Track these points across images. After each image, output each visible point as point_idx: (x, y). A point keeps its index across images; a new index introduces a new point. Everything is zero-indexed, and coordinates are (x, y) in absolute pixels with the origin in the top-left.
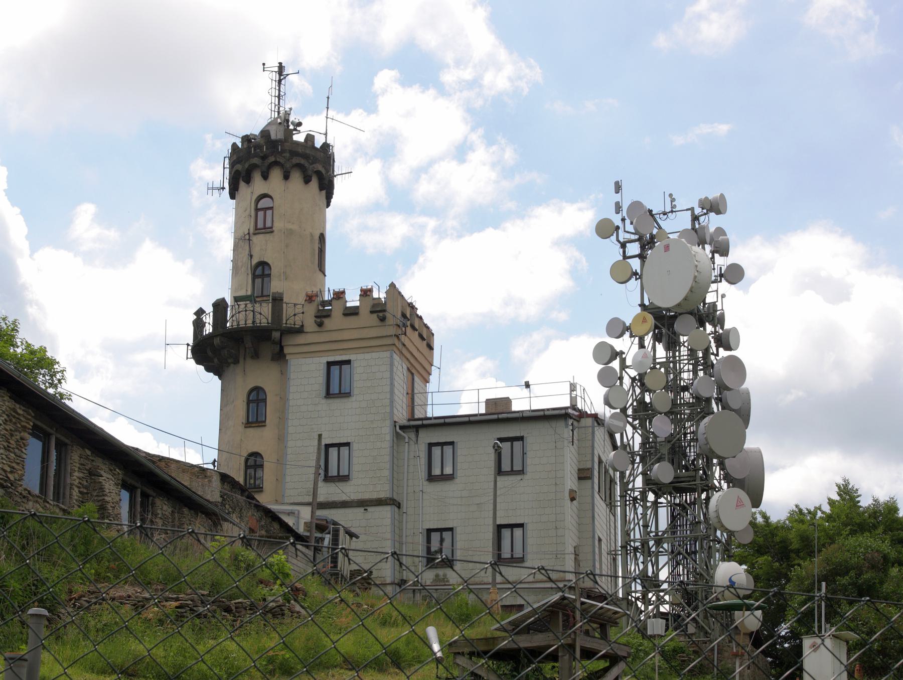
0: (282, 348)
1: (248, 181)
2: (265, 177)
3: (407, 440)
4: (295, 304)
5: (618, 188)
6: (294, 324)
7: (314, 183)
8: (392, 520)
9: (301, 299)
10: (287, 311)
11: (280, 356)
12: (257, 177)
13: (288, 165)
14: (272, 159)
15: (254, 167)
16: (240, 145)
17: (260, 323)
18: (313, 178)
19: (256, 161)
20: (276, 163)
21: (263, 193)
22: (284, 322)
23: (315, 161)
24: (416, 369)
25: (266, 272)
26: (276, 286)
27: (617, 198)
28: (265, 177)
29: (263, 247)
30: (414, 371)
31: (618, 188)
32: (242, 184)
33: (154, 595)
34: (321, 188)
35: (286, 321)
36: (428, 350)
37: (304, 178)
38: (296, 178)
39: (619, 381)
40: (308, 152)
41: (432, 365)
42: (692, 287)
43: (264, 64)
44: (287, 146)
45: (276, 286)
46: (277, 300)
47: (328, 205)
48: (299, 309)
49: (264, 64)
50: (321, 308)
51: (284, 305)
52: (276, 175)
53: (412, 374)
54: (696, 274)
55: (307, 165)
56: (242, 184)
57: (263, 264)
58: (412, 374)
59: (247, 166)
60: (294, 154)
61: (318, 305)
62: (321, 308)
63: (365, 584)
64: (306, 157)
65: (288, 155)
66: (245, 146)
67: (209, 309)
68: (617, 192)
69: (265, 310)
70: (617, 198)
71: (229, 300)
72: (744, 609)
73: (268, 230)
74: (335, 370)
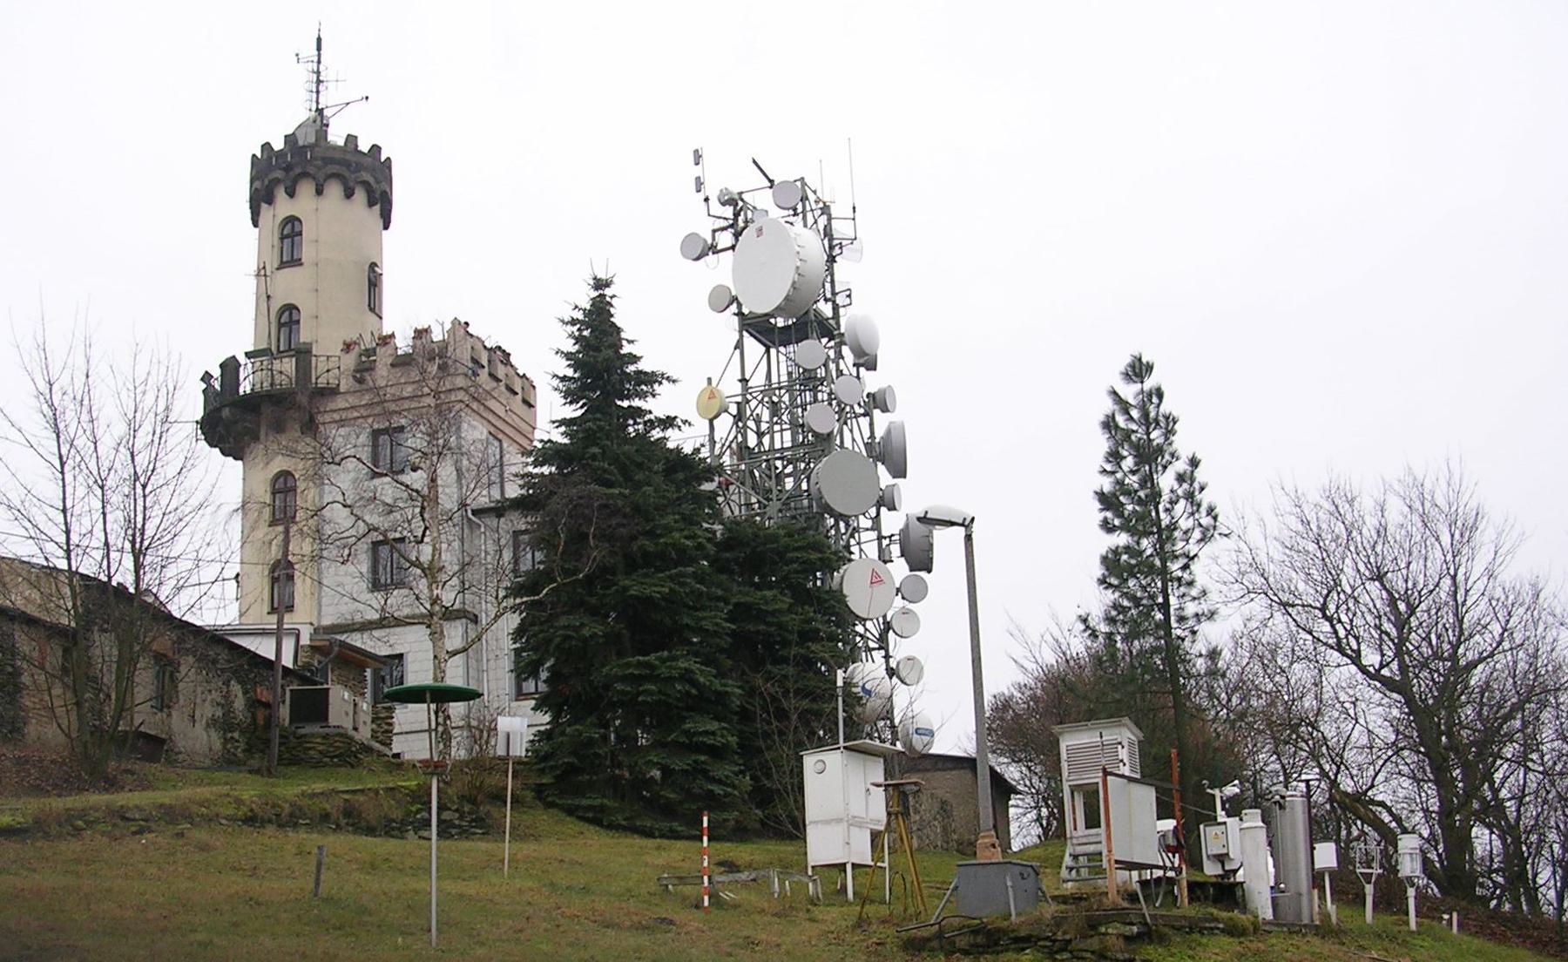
0: (312, 419)
1: (270, 201)
2: (291, 194)
3: (483, 530)
4: (328, 357)
5: (698, 157)
6: (328, 384)
7: (360, 196)
8: (349, 625)
9: (336, 349)
10: (319, 366)
11: (310, 426)
12: (281, 194)
13: (321, 176)
14: (298, 170)
15: (277, 181)
16: (259, 156)
17: (281, 385)
18: (356, 191)
19: (279, 174)
20: (305, 175)
21: (288, 214)
22: (314, 380)
23: (359, 167)
24: (504, 433)
25: (295, 318)
26: (305, 335)
27: (697, 171)
28: (291, 194)
29: (291, 286)
30: (500, 436)
31: (698, 157)
32: (264, 206)
33: (717, 753)
34: (382, 215)
35: (317, 379)
36: (525, 407)
37: (345, 191)
38: (334, 190)
39: (881, 469)
40: (348, 157)
41: (534, 428)
42: (794, 282)
43: (297, 55)
44: (319, 152)
45: (305, 335)
46: (303, 354)
47: (386, 227)
48: (333, 363)
49: (297, 55)
50: (364, 359)
51: (314, 359)
52: (306, 189)
53: (500, 441)
54: (799, 264)
55: (347, 174)
56: (264, 206)
57: (291, 308)
58: (500, 441)
59: (266, 182)
60: (327, 161)
61: (361, 355)
62: (364, 359)
63: (383, 725)
64: (347, 164)
65: (319, 163)
66: (265, 157)
67: (216, 372)
68: (697, 164)
69: (288, 365)
70: (697, 171)
71: (242, 359)
72: (428, 700)
73: (295, 262)
74: (384, 439)
